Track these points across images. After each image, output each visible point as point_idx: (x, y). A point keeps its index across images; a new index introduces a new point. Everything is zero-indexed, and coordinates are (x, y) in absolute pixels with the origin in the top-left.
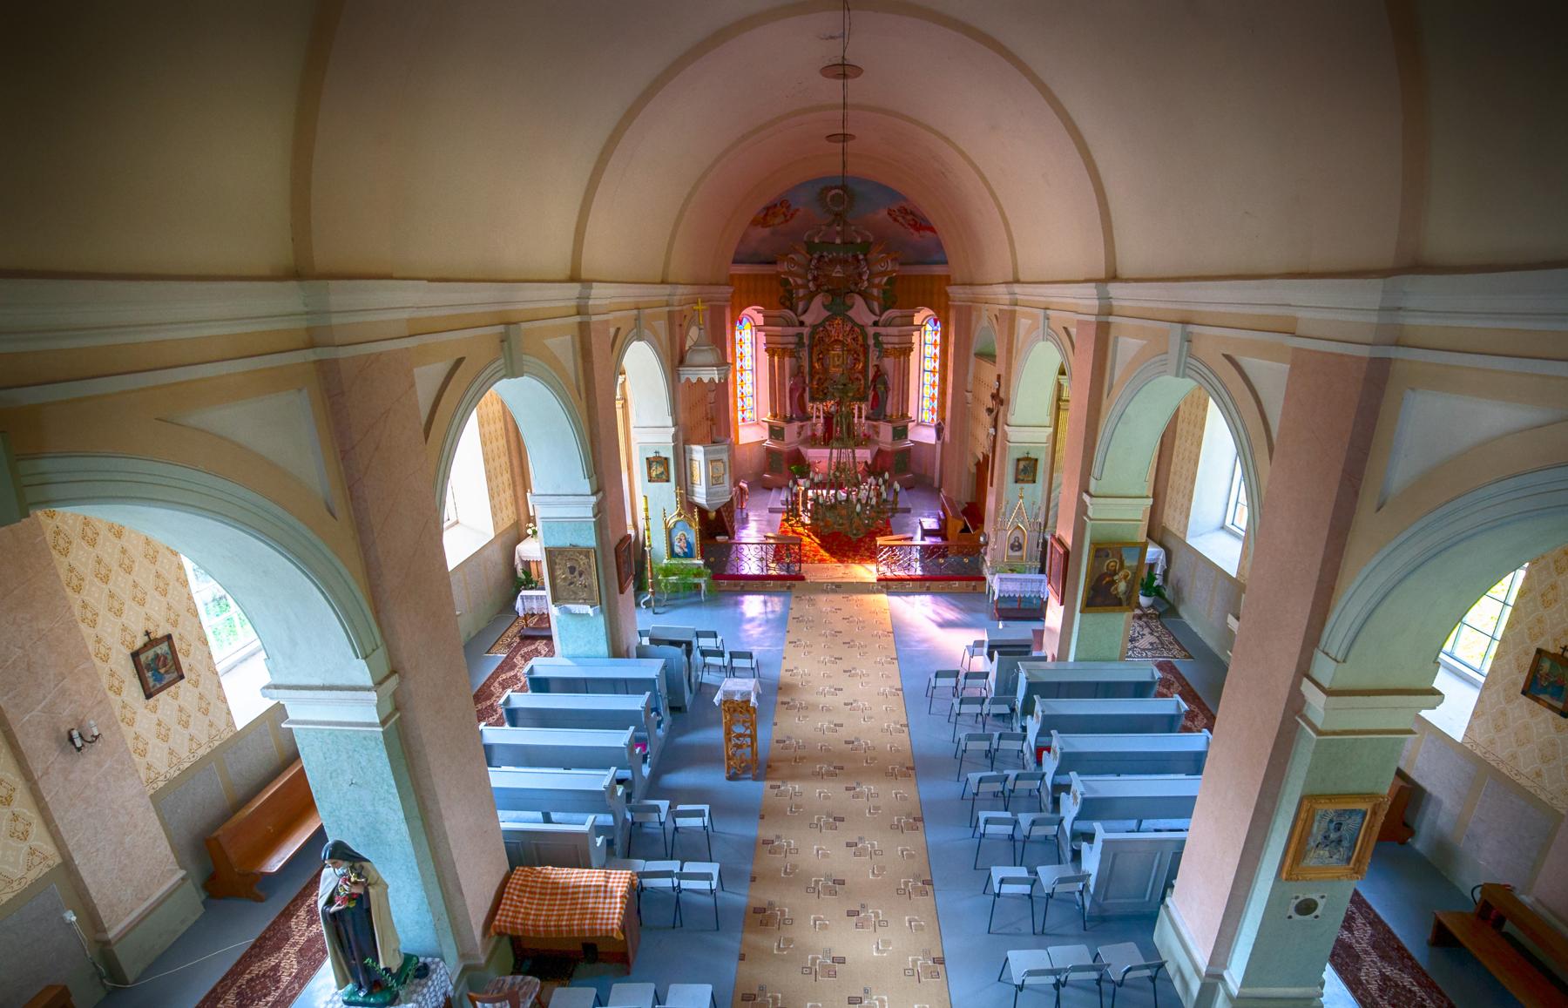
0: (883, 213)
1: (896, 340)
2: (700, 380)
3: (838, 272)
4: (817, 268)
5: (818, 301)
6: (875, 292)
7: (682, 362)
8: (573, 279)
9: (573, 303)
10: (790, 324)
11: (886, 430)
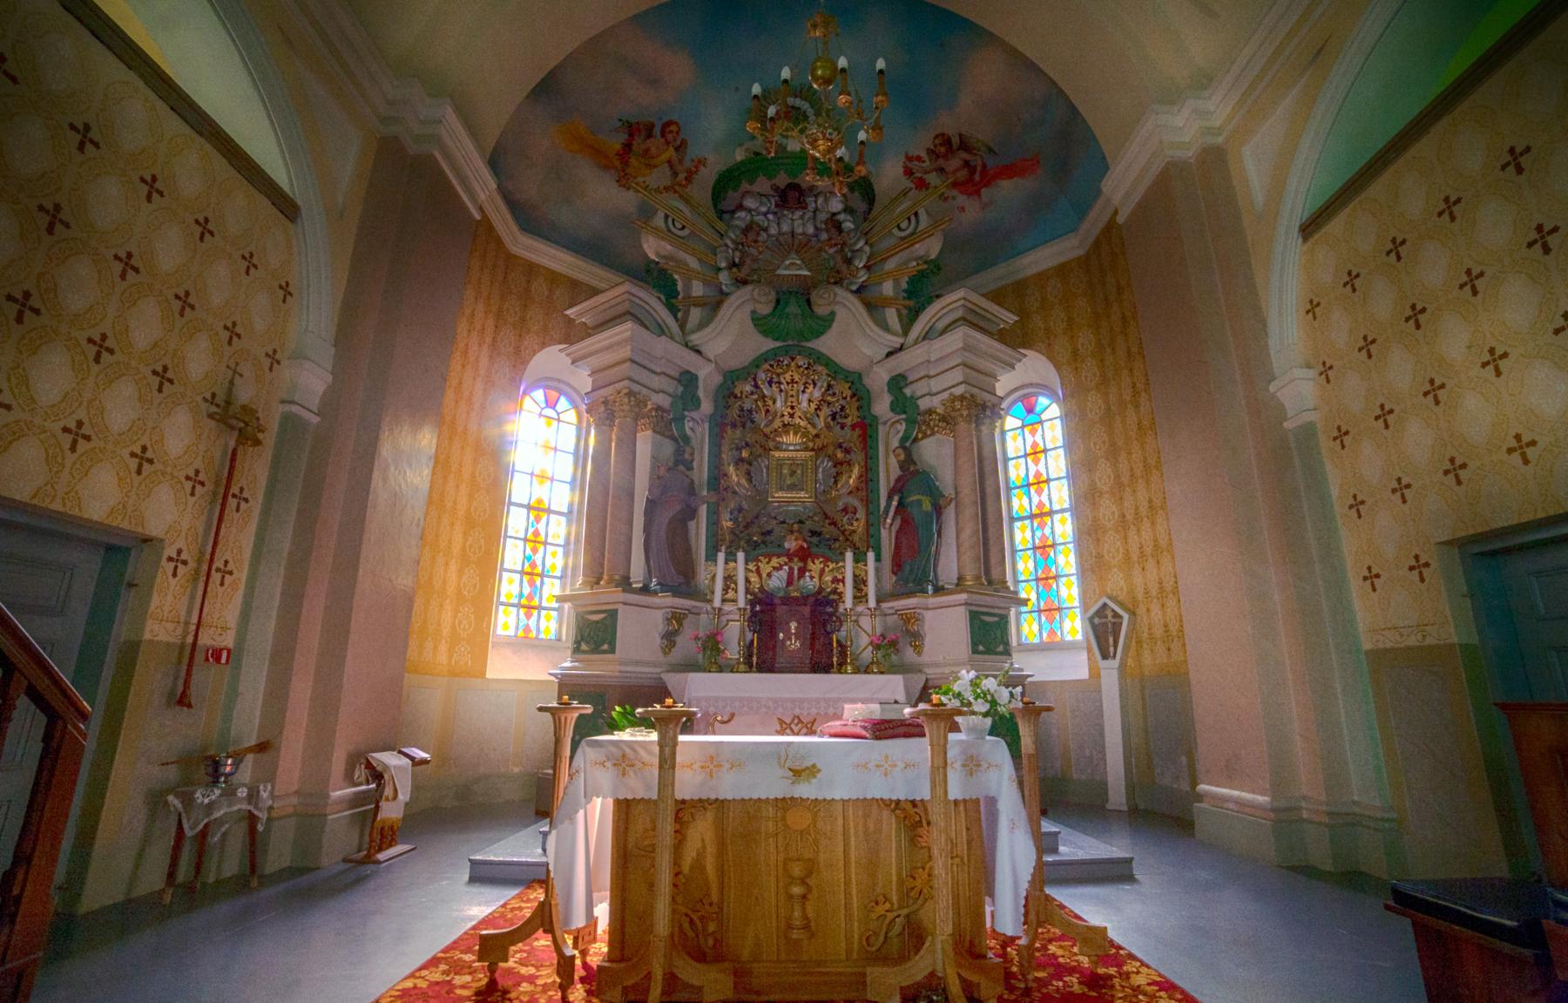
11: (945, 627)
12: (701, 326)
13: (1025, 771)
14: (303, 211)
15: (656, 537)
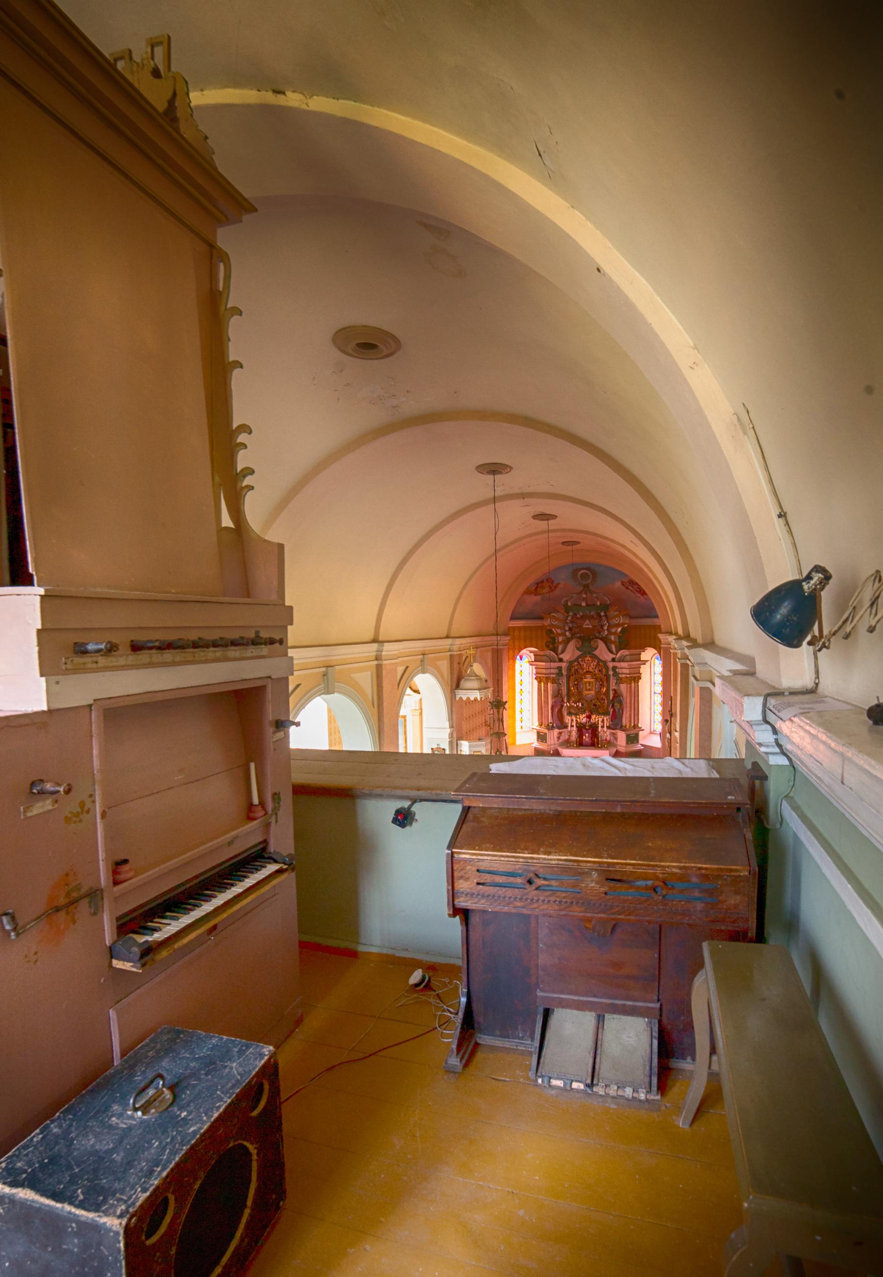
0: (618, 584)
1: (627, 671)
2: (468, 698)
3: (587, 625)
4: (572, 622)
5: (571, 645)
6: (613, 638)
7: (458, 686)
8: (375, 641)
9: (374, 654)
10: (552, 660)
11: (622, 736)
12: (563, 652)
13: (454, 714)
14: (152, 78)
15: (554, 714)
